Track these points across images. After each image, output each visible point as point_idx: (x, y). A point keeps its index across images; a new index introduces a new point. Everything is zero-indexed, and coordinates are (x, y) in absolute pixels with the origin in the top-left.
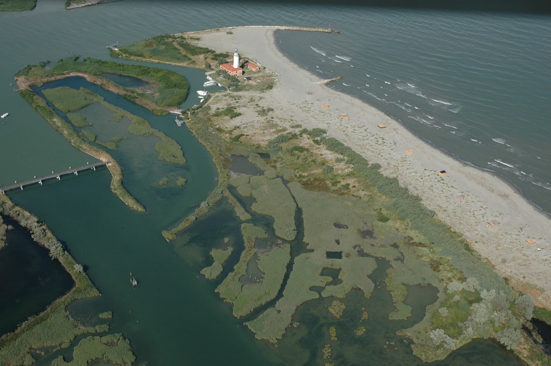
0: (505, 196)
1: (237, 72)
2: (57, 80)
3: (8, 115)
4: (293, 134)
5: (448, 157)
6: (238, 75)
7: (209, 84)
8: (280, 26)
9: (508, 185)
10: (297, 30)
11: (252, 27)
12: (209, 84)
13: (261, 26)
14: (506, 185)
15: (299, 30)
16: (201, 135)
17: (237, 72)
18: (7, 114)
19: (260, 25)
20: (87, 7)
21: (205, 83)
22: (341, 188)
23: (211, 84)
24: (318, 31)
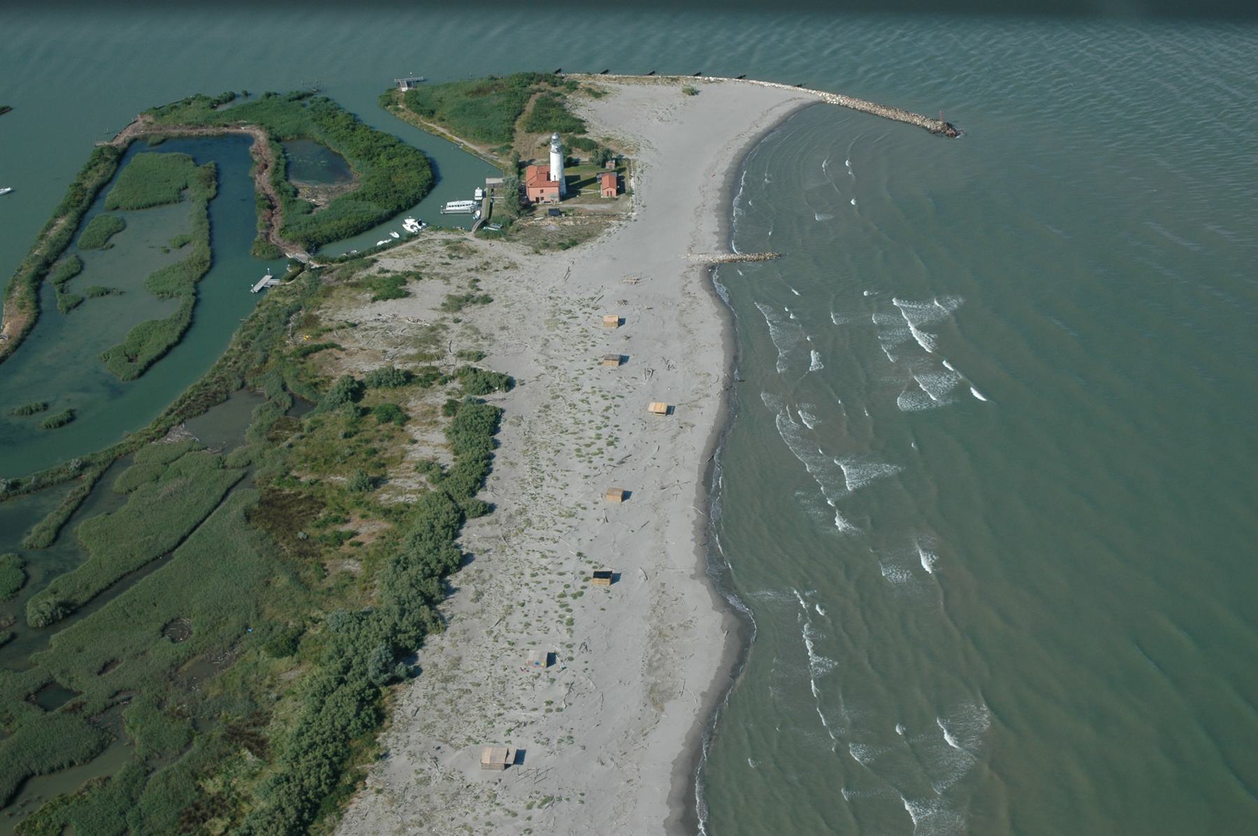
0: (657, 697)
1: (542, 191)
2: (203, 136)
3: (9, 192)
4: (397, 189)
5: (695, 552)
6: (546, 199)
7: (457, 208)
8: (830, 92)
9: (712, 682)
10: (866, 112)
11: (766, 84)
12: (457, 208)
13: (789, 87)
14: (712, 676)
15: (869, 113)
16: (257, 339)
17: (542, 191)
18: (9, 189)
19: (788, 84)
20: (201, 518)
21: (449, 204)
22: (344, 490)
23: (462, 208)
24: (910, 123)
